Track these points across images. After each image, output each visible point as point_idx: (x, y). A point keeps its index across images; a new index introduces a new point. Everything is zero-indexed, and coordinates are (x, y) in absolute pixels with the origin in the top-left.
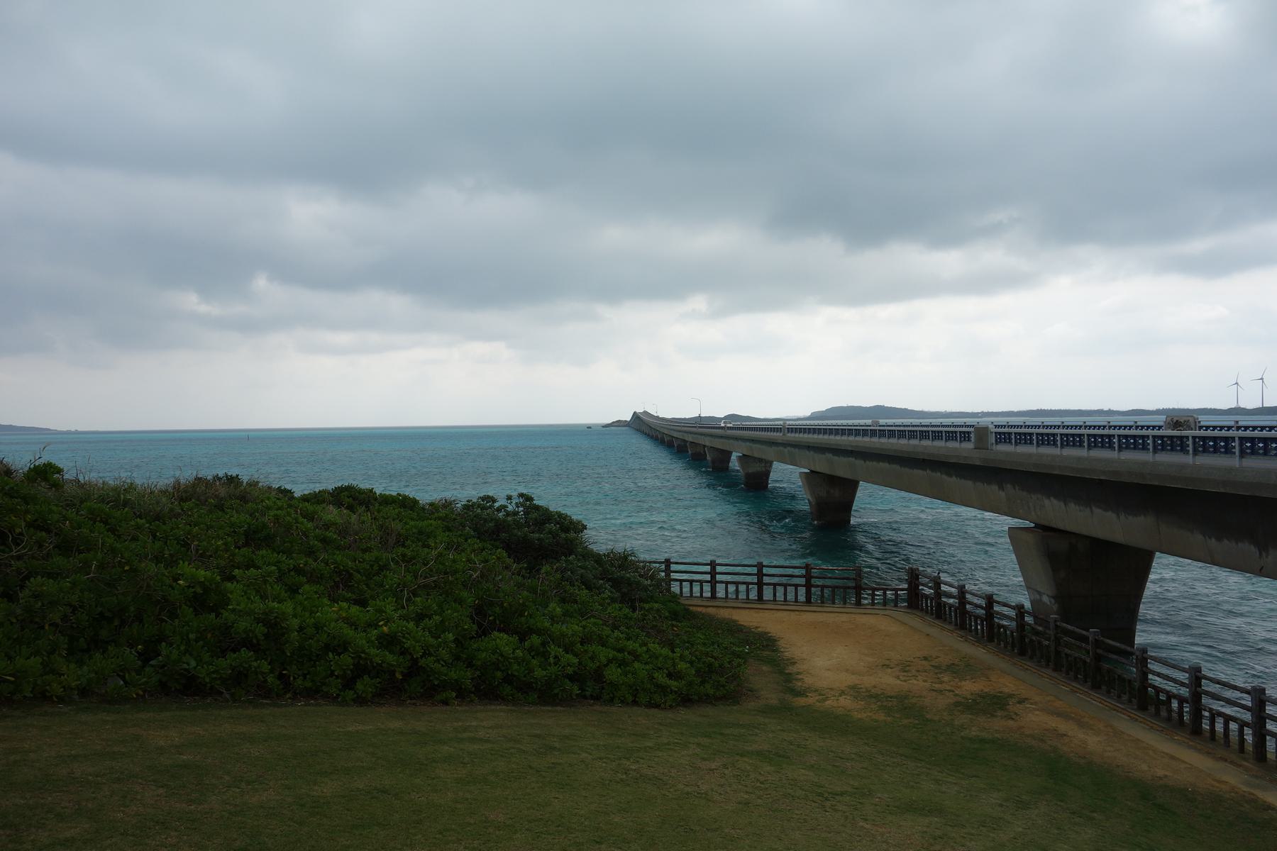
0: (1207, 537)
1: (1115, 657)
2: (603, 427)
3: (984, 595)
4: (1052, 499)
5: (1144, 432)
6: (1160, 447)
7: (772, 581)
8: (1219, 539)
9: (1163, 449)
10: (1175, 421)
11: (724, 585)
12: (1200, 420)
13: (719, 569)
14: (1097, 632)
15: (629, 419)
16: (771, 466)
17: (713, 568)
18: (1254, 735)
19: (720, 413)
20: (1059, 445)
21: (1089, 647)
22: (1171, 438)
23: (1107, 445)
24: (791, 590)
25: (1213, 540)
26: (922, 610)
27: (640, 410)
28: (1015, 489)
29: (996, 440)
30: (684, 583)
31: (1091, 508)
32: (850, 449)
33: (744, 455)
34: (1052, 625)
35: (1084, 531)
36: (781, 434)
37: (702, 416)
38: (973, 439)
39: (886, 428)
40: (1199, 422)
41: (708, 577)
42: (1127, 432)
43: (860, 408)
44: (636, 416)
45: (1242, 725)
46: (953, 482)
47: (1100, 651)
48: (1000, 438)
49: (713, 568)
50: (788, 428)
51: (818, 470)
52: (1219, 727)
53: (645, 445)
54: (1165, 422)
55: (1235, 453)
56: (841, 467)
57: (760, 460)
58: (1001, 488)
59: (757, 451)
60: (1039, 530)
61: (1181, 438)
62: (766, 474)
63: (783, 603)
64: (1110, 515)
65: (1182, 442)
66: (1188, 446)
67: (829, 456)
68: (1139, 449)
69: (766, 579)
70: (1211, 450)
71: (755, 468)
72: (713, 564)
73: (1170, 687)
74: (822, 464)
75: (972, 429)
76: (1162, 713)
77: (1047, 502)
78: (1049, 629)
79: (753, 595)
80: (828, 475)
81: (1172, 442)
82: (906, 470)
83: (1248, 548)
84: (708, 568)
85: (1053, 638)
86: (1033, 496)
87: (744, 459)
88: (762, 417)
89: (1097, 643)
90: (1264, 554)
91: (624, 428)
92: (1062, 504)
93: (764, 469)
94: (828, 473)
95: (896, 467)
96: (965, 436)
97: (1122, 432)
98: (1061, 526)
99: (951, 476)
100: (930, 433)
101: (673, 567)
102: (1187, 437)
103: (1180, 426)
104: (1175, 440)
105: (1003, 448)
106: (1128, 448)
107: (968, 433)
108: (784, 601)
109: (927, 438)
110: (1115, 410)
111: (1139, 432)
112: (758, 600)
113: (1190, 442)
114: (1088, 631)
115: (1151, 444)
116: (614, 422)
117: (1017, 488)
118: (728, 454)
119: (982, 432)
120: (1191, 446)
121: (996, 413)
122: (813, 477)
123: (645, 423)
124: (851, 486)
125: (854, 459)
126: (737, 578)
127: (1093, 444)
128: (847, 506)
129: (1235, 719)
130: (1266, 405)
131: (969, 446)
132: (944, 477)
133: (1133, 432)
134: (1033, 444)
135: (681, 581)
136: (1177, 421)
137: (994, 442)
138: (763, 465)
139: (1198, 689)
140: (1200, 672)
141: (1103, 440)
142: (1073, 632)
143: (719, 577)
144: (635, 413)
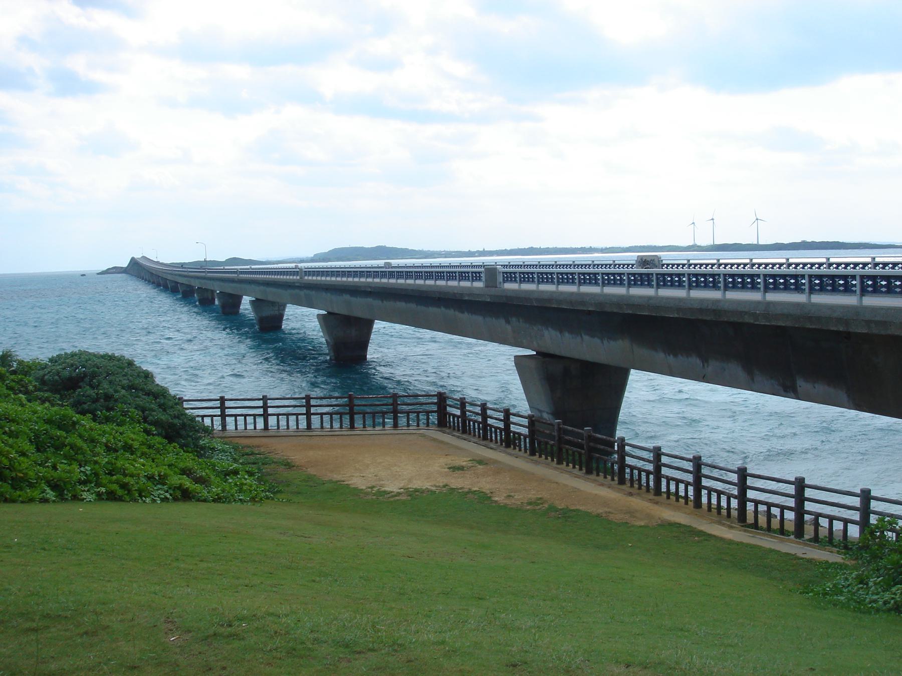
0: (667, 355)
1: (602, 447)
2: (98, 274)
3: (502, 410)
4: (550, 329)
5: (621, 270)
6: (633, 283)
7: (319, 411)
8: (675, 355)
9: (635, 284)
10: (644, 260)
11: (276, 417)
12: (662, 259)
13: (227, 404)
14: (590, 429)
15: (126, 266)
16: (284, 310)
17: (308, 402)
18: (694, 490)
19: (221, 256)
20: (556, 283)
21: (584, 442)
22: (641, 275)
23: (571, 281)
24: (292, 419)
25: (671, 356)
26: (450, 427)
27: (138, 256)
28: (519, 322)
29: (504, 279)
30: (238, 418)
31: (581, 336)
32: (370, 290)
33: (257, 299)
34: (556, 427)
35: (576, 355)
36: (298, 278)
37: (207, 260)
38: (483, 279)
39: (372, 270)
40: (662, 261)
41: (218, 412)
42: (608, 270)
43: (362, 248)
44: (134, 262)
45: (687, 484)
46: (465, 317)
47: (592, 444)
48: (507, 277)
49: (308, 402)
50: (305, 271)
51: (336, 312)
52: (673, 488)
53: (145, 291)
54: (636, 261)
55: (685, 286)
56: (358, 307)
57: (273, 303)
58: (508, 322)
59: (271, 294)
60: (540, 357)
61: (648, 275)
62: (279, 318)
63: (329, 430)
64: (597, 341)
65: (648, 277)
66: (653, 281)
67: (347, 297)
68: (668, 286)
69: (228, 412)
70: (711, 285)
71: (268, 312)
72: (265, 399)
73: (640, 464)
74: (341, 305)
75: (482, 269)
76: (635, 485)
77: (546, 333)
78: (554, 432)
79: (303, 424)
80: (345, 316)
81: (641, 277)
82: (422, 308)
83: (695, 361)
84: (260, 403)
85: (557, 438)
86: (535, 328)
87: (257, 304)
88: (786, 242)
89: (590, 438)
90: (706, 365)
91: (120, 275)
92: (558, 334)
93: (277, 312)
94: (347, 314)
95: (412, 306)
96: (476, 276)
97: (604, 270)
98: (557, 353)
99: (463, 312)
100: (395, 273)
101: (227, 404)
102: (652, 274)
103: (648, 264)
104: (637, 276)
105: (509, 286)
106: (609, 284)
107: (479, 273)
108: (321, 428)
109: (442, 278)
110: (847, 242)
111: (617, 270)
112: (307, 429)
113: (654, 278)
114: (583, 430)
115: (626, 280)
116: (109, 269)
117: (521, 320)
118: (237, 300)
119: (491, 271)
120: (655, 281)
121: (560, 249)
122: (329, 321)
123: (144, 269)
124: (366, 326)
125: (371, 300)
126: (244, 411)
127: (606, 282)
128: (363, 344)
129: (682, 482)
130: (717, 242)
131: (479, 285)
132: (457, 313)
133: (612, 270)
134: (535, 282)
135: (236, 416)
136: (646, 260)
137: (502, 281)
138: (277, 308)
139: (660, 463)
140: (660, 450)
141: (614, 277)
142: (572, 431)
143: (270, 411)
144: (133, 259)
